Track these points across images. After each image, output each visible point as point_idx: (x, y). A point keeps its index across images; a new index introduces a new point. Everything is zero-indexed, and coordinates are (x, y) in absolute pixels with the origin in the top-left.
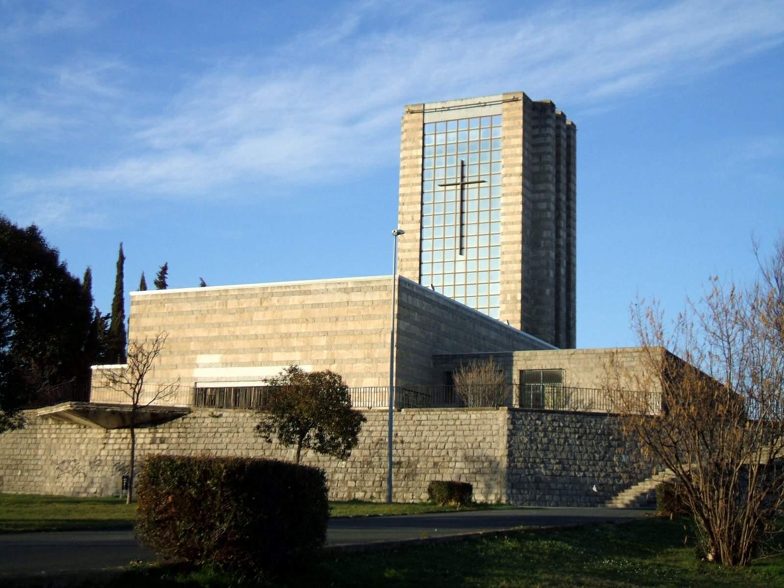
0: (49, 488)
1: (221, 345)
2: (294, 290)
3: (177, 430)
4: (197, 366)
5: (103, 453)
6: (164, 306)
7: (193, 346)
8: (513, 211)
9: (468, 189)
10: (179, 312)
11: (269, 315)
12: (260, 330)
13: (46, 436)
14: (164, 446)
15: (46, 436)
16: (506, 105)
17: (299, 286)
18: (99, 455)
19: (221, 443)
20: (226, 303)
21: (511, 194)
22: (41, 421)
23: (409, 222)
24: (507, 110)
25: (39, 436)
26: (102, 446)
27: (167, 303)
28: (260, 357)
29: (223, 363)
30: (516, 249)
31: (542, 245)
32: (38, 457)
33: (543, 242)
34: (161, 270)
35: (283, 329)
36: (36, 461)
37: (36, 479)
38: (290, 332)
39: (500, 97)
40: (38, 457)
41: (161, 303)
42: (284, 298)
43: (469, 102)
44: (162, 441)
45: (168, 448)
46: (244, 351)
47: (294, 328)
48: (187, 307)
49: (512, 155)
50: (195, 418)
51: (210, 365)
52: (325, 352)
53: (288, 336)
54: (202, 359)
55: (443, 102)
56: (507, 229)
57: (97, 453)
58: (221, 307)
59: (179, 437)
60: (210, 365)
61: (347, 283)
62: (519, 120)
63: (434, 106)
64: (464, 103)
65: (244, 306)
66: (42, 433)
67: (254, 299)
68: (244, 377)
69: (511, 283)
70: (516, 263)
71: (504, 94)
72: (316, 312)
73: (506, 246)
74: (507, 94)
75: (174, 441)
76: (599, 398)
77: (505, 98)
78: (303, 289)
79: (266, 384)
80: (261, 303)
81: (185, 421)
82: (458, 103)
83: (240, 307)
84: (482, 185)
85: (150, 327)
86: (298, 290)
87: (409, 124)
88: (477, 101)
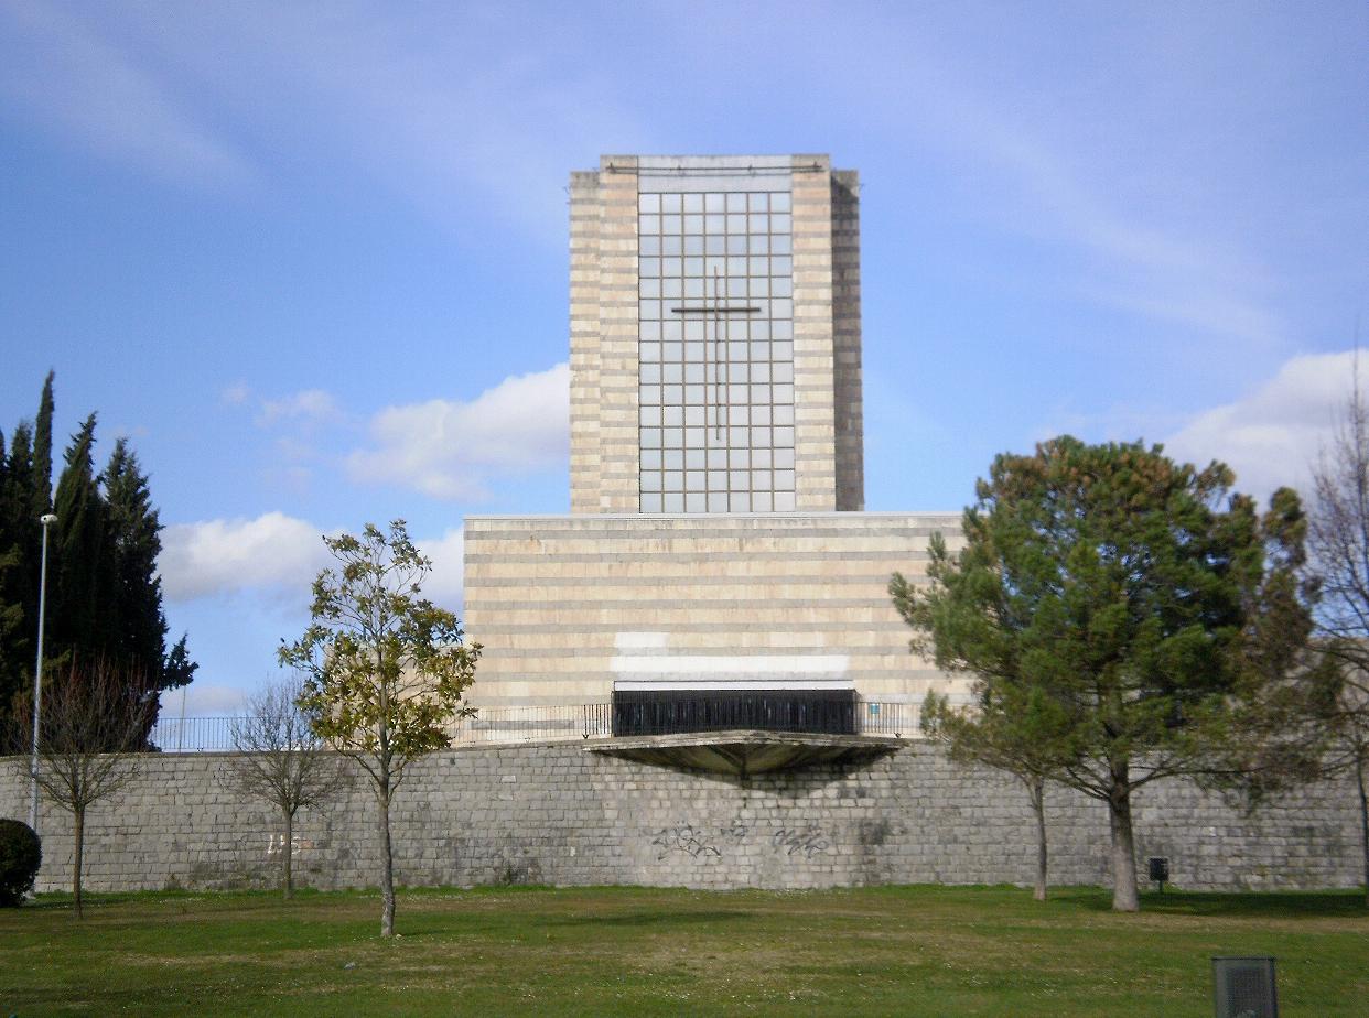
0: (644, 876)
1: (665, 617)
2: (806, 527)
3: (885, 775)
4: (617, 652)
5: (745, 814)
6: (540, 544)
7: (605, 617)
8: (816, 366)
9: (705, 320)
10: (571, 555)
11: (758, 568)
12: (742, 593)
13: (613, 786)
14: (869, 802)
15: (613, 786)
16: (798, 177)
17: (814, 520)
18: (739, 817)
19: (977, 796)
20: (670, 543)
21: (813, 337)
22: (595, 760)
23: (614, 373)
24: (801, 185)
25: (597, 786)
26: (741, 803)
27: (544, 538)
28: (746, 639)
29: (670, 649)
30: (823, 435)
31: (850, 427)
32: (605, 823)
33: (850, 421)
34: (80, 430)
35: (788, 592)
36: (606, 830)
37: (613, 861)
38: (802, 598)
39: (785, 161)
40: (605, 823)
41: (532, 538)
42: (787, 539)
43: (727, 162)
44: (862, 793)
45: (876, 804)
46: (713, 628)
47: (808, 592)
48: (589, 547)
49: (812, 268)
50: (914, 755)
51: (644, 652)
52: (872, 634)
53: (797, 605)
54: (623, 640)
55: (676, 157)
56: (806, 397)
57: (734, 813)
58: (660, 551)
59: (893, 787)
60: (644, 652)
61: (906, 519)
62: (824, 206)
63: (657, 163)
64: (717, 163)
65: (708, 550)
66: (602, 781)
67: (725, 539)
68: (759, 673)
69: (817, 493)
70: (825, 459)
71: (794, 156)
72: (851, 568)
73: (806, 427)
74: (801, 156)
75: (884, 793)
76: (738, 569)
77: (797, 163)
78: (821, 525)
79: (168, 651)
80: (741, 548)
81: (896, 759)
82: (706, 163)
83: (699, 551)
84: (678, 305)
85: (510, 580)
86: (812, 526)
87: (610, 192)
88: (745, 162)
